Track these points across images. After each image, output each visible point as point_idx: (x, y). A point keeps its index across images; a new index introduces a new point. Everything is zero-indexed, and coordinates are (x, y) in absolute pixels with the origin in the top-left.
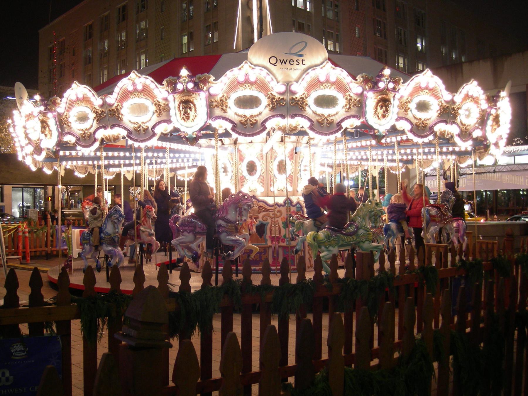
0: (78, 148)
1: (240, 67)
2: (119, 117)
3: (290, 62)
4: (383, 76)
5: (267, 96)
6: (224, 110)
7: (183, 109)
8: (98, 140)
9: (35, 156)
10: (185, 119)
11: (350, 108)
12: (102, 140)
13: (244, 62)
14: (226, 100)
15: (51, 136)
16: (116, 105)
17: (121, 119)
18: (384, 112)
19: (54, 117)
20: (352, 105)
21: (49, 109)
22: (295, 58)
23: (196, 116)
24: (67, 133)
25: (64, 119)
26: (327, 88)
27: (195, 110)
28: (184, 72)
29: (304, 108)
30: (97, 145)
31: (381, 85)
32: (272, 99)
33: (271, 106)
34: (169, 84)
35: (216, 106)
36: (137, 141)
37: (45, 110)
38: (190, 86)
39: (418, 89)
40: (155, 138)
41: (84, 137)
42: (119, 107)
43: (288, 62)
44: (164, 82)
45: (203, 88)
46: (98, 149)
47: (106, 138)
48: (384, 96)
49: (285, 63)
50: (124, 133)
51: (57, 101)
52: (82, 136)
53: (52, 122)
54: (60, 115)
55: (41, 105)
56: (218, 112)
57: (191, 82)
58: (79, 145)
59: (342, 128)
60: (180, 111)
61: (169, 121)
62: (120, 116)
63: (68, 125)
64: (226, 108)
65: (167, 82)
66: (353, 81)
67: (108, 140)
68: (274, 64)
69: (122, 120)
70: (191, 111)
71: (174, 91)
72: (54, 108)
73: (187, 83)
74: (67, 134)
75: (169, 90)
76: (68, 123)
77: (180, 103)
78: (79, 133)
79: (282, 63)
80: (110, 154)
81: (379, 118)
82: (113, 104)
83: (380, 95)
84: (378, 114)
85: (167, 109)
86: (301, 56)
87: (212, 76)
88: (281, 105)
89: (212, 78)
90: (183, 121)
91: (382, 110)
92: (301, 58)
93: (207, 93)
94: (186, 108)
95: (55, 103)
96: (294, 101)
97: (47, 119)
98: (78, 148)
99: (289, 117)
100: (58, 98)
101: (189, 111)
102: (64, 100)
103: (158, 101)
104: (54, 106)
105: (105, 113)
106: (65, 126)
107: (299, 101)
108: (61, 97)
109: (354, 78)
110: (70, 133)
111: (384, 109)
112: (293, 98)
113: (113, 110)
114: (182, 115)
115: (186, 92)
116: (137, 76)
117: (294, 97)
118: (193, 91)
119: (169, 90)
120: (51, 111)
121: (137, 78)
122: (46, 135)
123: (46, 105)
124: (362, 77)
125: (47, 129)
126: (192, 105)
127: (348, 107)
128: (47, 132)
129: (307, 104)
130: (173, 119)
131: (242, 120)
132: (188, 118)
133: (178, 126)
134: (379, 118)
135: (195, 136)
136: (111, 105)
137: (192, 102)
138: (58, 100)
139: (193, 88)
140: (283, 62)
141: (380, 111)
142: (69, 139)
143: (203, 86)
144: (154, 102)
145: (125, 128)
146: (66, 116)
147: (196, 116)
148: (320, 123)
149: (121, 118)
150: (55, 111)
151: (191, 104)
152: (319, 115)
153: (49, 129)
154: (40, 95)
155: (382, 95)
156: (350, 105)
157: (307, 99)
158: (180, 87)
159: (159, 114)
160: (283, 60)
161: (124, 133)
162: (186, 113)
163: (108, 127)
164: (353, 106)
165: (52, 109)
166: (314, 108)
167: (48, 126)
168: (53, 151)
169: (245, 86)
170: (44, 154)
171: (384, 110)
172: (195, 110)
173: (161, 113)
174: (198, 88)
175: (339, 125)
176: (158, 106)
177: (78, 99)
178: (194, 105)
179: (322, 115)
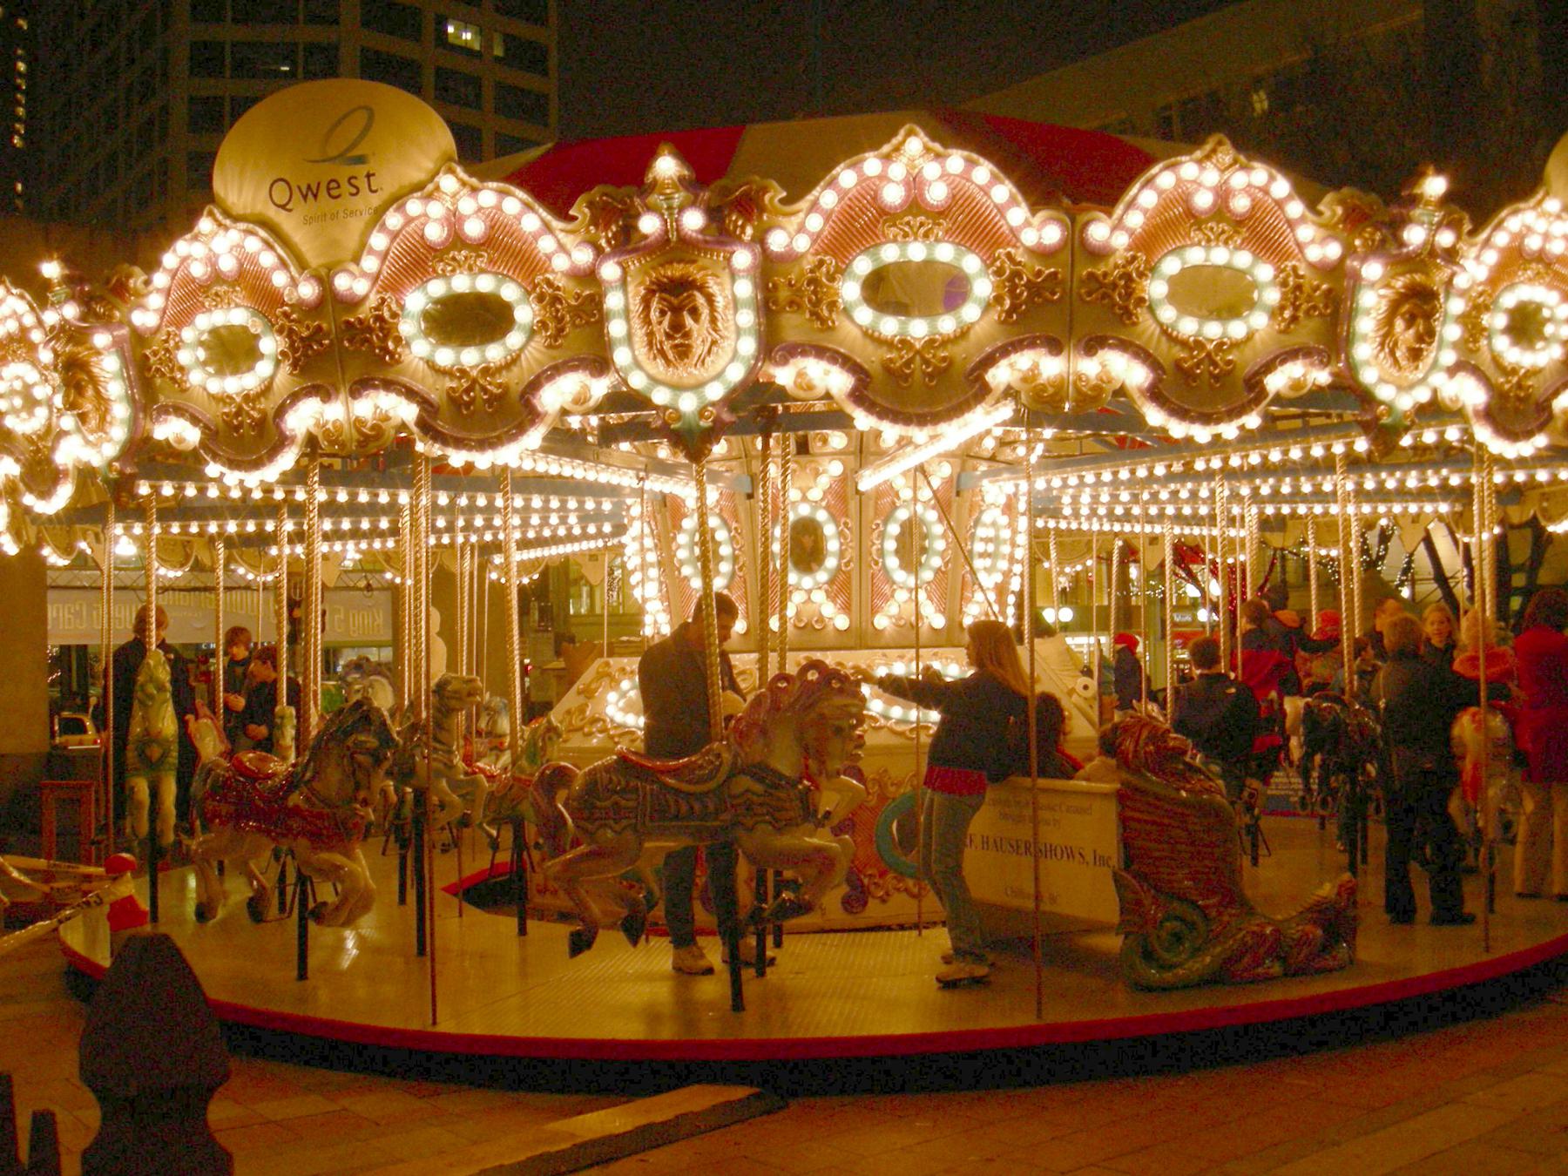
0: (213, 469)
1: (886, 148)
2: (386, 350)
3: (329, 189)
4: (1414, 200)
5: (992, 264)
6: (823, 320)
7: (663, 313)
8: (292, 439)
9: (29, 499)
10: (671, 355)
11: (1294, 319)
12: (311, 441)
13: (902, 132)
14: (832, 279)
15: (103, 420)
16: (373, 301)
17: (392, 357)
18: (1420, 338)
19: (117, 344)
20: (1304, 307)
21: (98, 316)
22: (343, 173)
23: (714, 343)
24: (165, 410)
25: (155, 354)
26: (1217, 239)
27: (713, 320)
28: (666, 166)
29: (1129, 314)
30: (287, 460)
31: (1414, 236)
32: (1009, 280)
33: (1007, 303)
34: (602, 215)
35: (791, 303)
36: (459, 443)
37: (83, 318)
38: (693, 221)
39: (1516, 260)
40: (535, 437)
41: (237, 428)
42: (172, 343)
43: (323, 193)
44: (580, 209)
45: (743, 232)
46: (297, 476)
47: (327, 433)
48: (1418, 277)
49: (315, 196)
50: (407, 412)
51: (131, 282)
52: (228, 424)
53: (109, 366)
54: (139, 338)
55: (67, 300)
56: (794, 326)
57: (693, 204)
58: (215, 457)
59: (1267, 395)
60: (647, 321)
61: (600, 363)
62: (391, 345)
63: (173, 379)
64: (831, 311)
65: (591, 205)
66: (1309, 215)
67: (332, 443)
68: (283, 207)
69: (398, 362)
70: (696, 320)
71: (626, 240)
72: (117, 314)
73: (682, 209)
74: (167, 412)
75: (603, 242)
76: (172, 370)
77: (651, 292)
78: (214, 413)
79: (305, 197)
80: (342, 496)
81: (1396, 361)
82: (365, 298)
83: (1403, 274)
84: (1396, 344)
85: (591, 312)
86: (361, 160)
87: (774, 183)
88: (1047, 301)
89: (775, 194)
90: (660, 361)
91: (1411, 331)
92: (361, 170)
93: (758, 249)
94: (677, 311)
95: (120, 291)
96: (1094, 285)
97: (90, 356)
98: (213, 469)
99: (1076, 346)
100: (137, 270)
101: (689, 321)
102: (160, 279)
103: (549, 283)
104: (117, 301)
105: (327, 335)
106: (158, 381)
107: (1115, 286)
108: (152, 265)
109: (1312, 204)
110: (179, 411)
111: (1420, 325)
112: (1091, 276)
113: (360, 321)
114: (659, 336)
115: (674, 246)
116: (464, 184)
117: (1100, 270)
118: (706, 242)
119: (603, 242)
120: (106, 322)
121: (465, 191)
122: (83, 418)
123: (86, 301)
124: (1342, 202)
125: (90, 392)
126: (700, 300)
127: (1287, 314)
128: (88, 407)
129: (1141, 300)
130: (621, 356)
131: (891, 360)
132: (683, 352)
133: (637, 381)
134: (1396, 361)
135: (704, 424)
136: (354, 303)
137: (702, 288)
138: (137, 280)
139: (702, 231)
140: (311, 193)
141: (1405, 334)
142: (175, 430)
143: (740, 223)
144: (535, 286)
145: (410, 394)
146: (166, 341)
147: (714, 343)
148: (1184, 374)
149: (392, 355)
150: (121, 324)
151: (697, 294)
152: (1184, 344)
153: (98, 393)
154: (67, 261)
155: (1410, 272)
156: (1296, 308)
157: (1146, 283)
158: (649, 224)
159: (555, 337)
160: (309, 187)
161: (407, 412)
162: (677, 327)
163: (337, 391)
164: (1307, 313)
165: (111, 317)
166: (1167, 314)
167: (94, 380)
168: (107, 481)
169: (908, 223)
170: (63, 495)
171: (1421, 328)
172: (713, 320)
173: (562, 330)
174: (721, 234)
175: (1254, 385)
176: (552, 304)
177: (217, 277)
178: (710, 299)
179: (1197, 342)
